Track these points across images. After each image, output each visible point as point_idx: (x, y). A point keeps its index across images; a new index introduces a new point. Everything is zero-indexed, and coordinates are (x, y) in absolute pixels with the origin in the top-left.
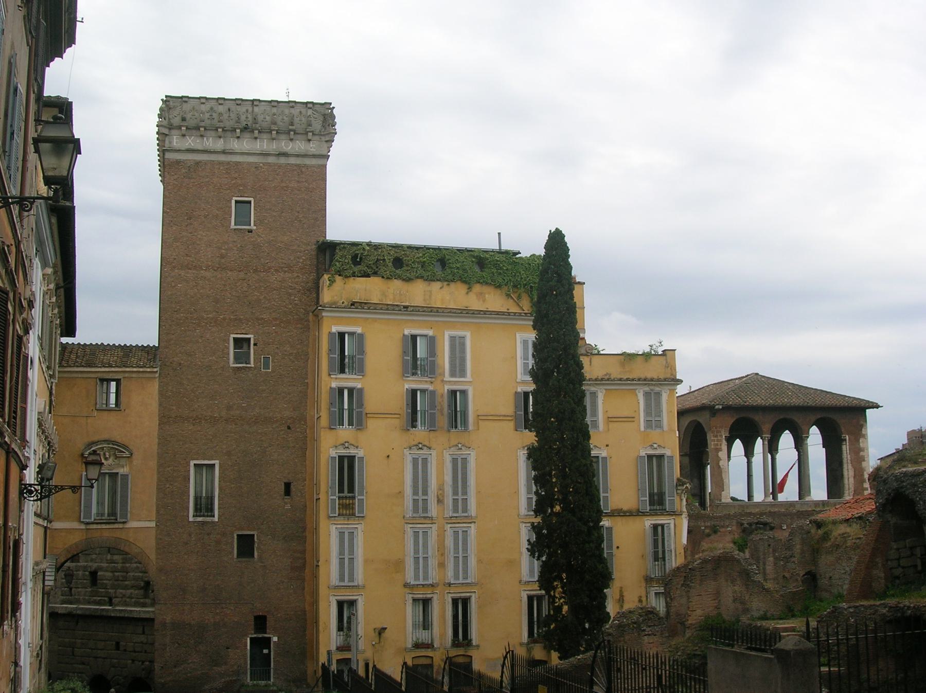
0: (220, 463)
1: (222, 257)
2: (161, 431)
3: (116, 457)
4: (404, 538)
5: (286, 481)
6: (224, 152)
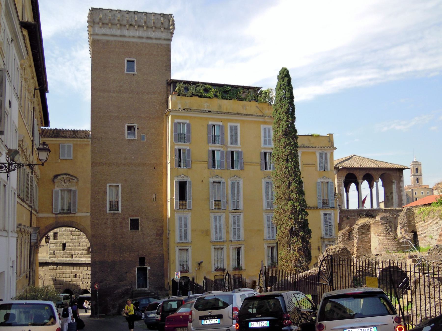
0: (121, 185)
1: (121, 86)
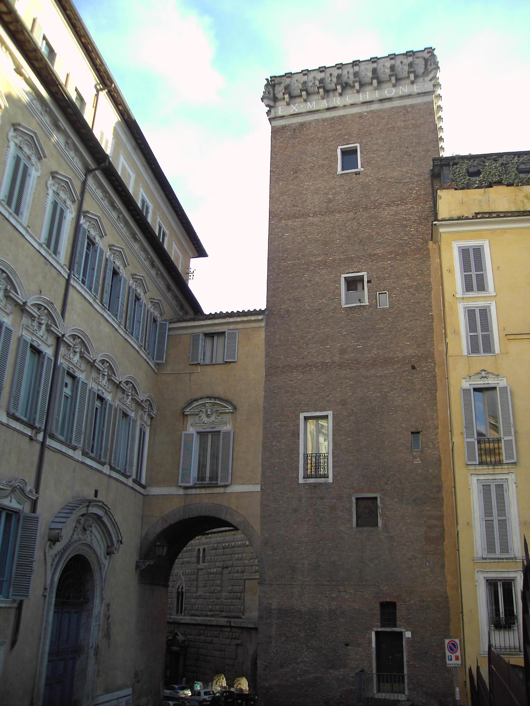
1: (330, 201)
2: (268, 382)
6: (328, 109)
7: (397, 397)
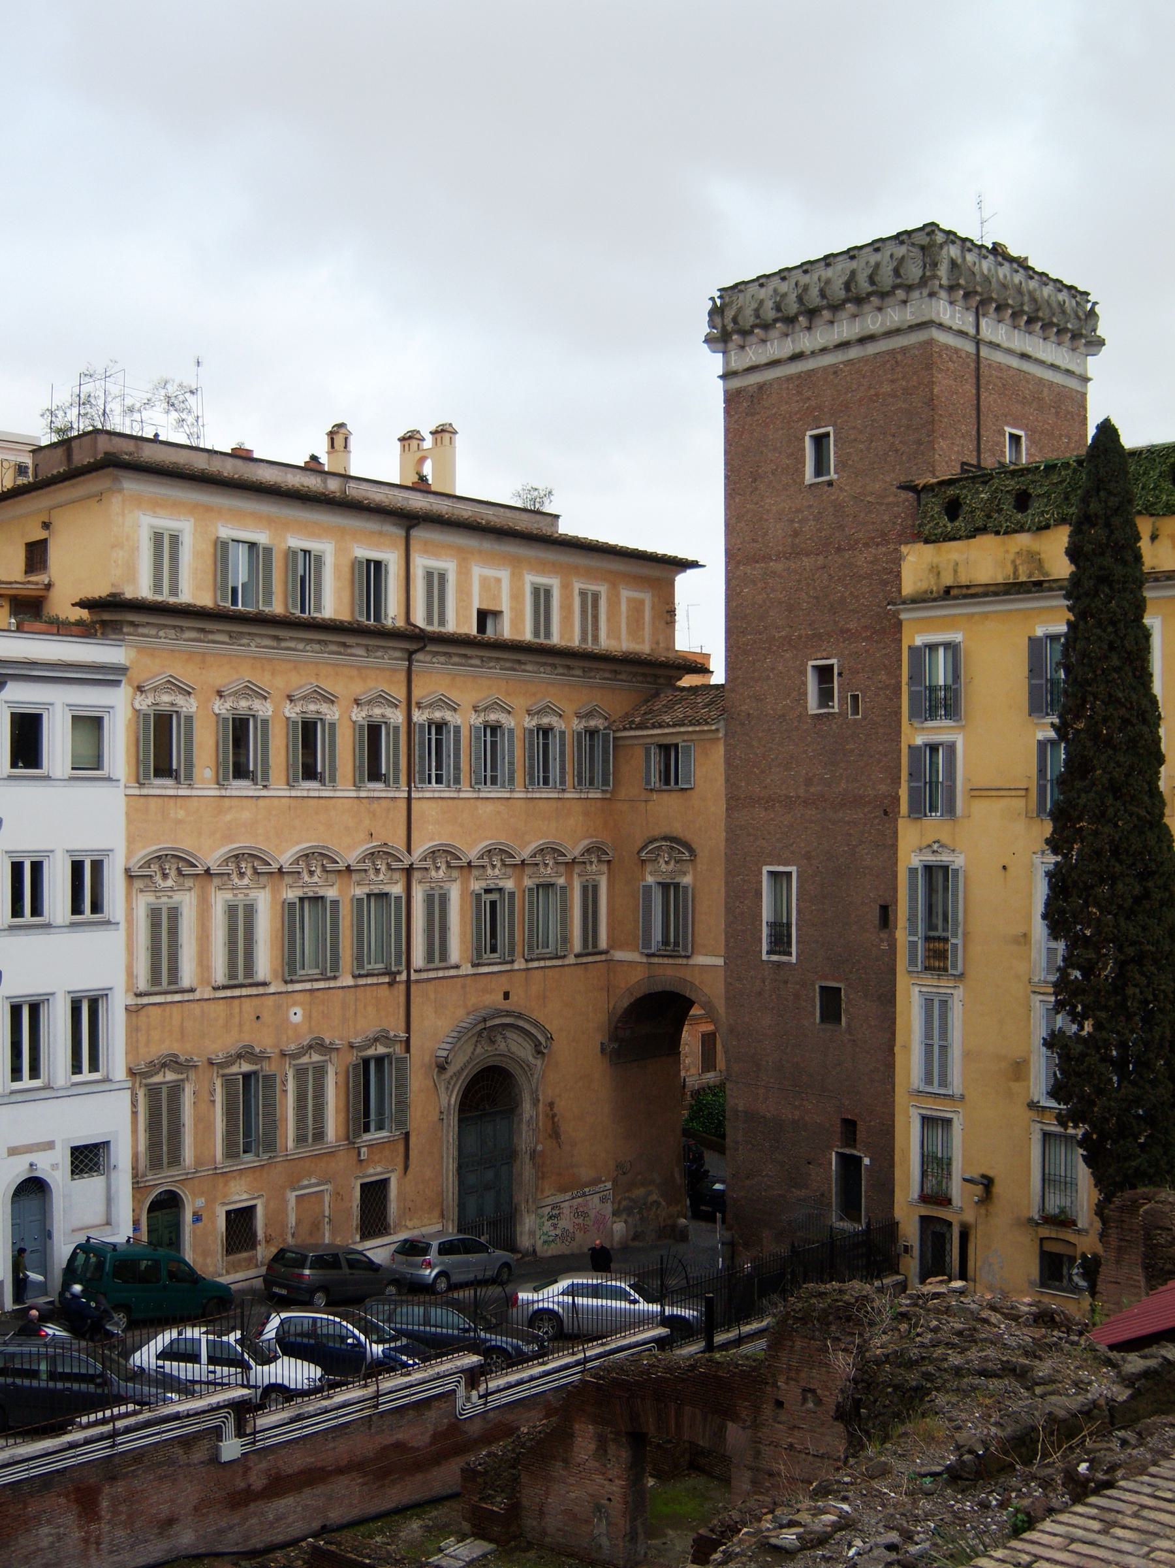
0: (798, 871)
1: (796, 534)
3: (677, 862)
4: (1029, 1016)
5: (882, 903)
7: (867, 854)
